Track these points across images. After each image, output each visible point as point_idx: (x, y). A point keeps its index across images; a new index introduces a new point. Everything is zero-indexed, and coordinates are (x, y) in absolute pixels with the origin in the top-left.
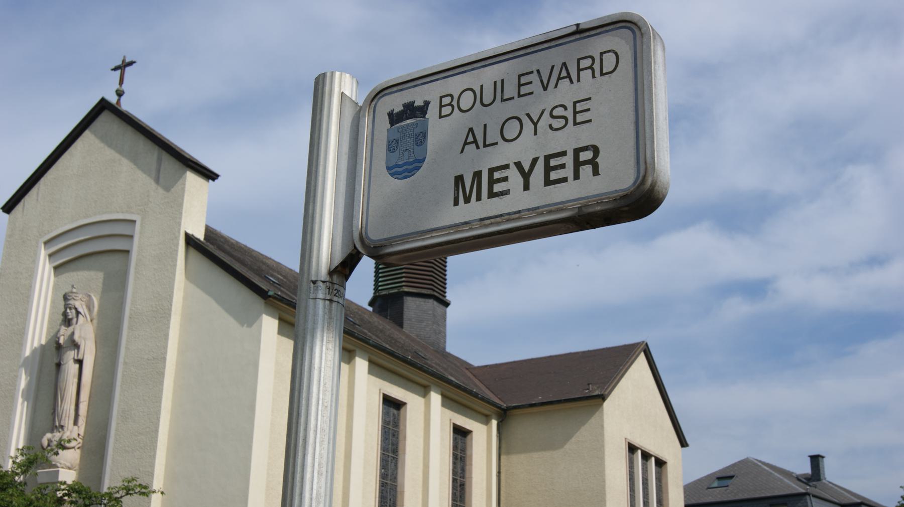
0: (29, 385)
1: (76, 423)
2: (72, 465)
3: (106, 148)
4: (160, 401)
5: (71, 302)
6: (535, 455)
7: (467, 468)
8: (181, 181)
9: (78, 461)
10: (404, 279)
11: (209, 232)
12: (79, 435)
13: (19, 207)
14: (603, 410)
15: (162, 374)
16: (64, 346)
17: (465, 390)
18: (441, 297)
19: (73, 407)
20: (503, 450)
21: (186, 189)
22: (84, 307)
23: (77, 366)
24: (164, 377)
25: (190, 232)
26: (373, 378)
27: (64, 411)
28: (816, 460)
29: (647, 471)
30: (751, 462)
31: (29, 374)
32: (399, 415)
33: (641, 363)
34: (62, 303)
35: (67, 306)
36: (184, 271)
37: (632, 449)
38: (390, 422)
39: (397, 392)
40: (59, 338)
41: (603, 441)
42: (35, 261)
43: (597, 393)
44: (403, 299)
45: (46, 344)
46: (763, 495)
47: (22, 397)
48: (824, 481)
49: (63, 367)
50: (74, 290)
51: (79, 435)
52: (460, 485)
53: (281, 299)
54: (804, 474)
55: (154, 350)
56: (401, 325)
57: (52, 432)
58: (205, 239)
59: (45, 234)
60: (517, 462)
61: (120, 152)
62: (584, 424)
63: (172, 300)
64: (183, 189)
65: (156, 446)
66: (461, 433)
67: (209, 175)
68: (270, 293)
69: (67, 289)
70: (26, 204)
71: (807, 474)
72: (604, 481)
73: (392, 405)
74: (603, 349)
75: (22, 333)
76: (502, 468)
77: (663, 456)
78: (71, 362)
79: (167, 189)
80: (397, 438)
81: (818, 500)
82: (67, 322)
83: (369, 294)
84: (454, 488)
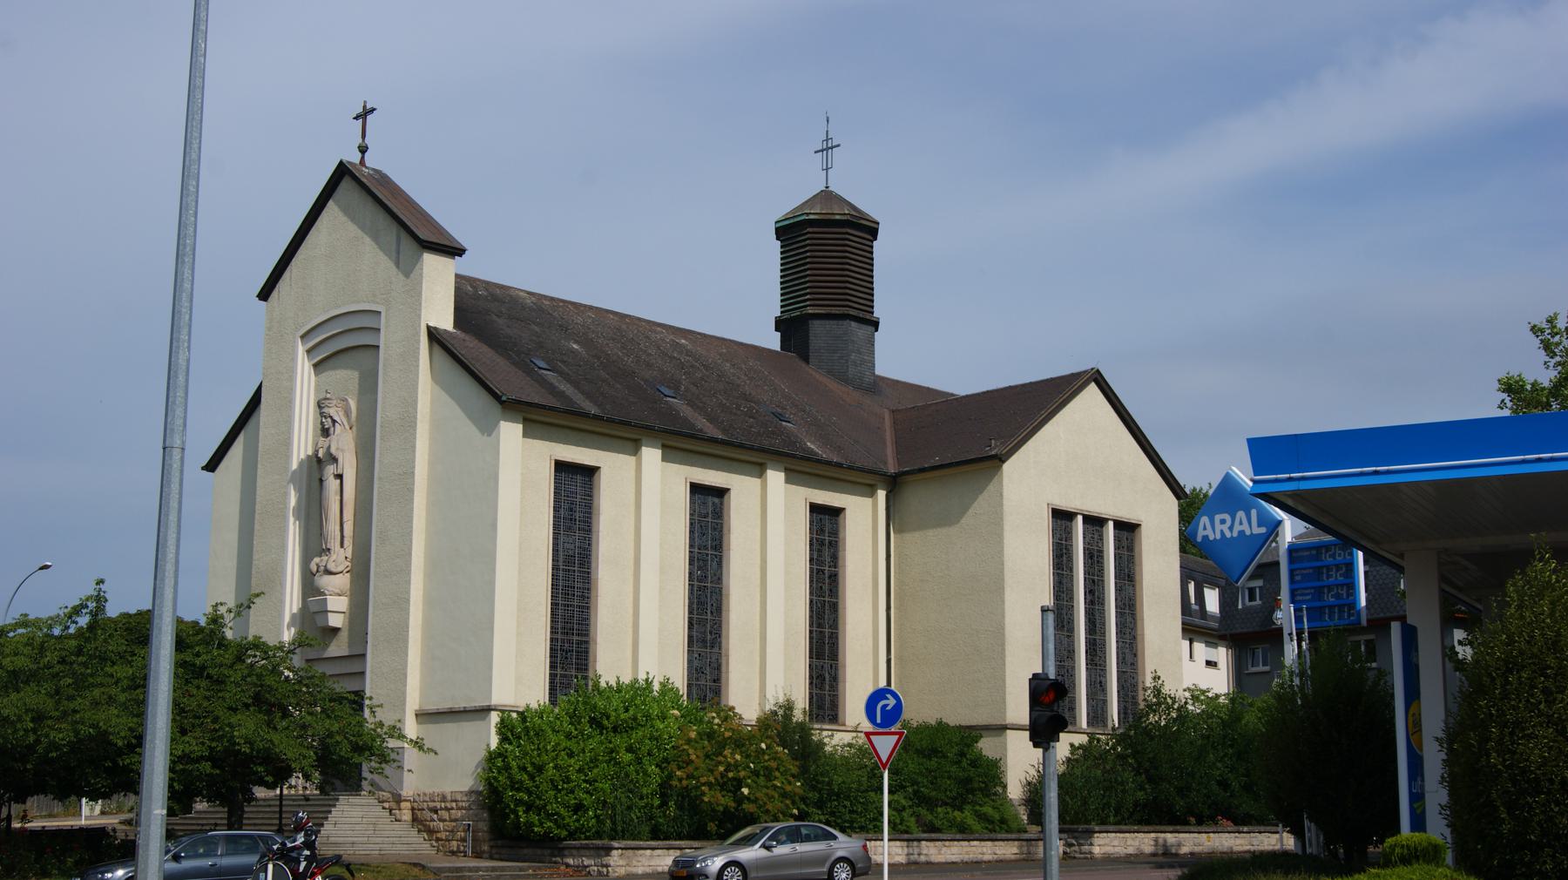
1: (342, 546)
2: (342, 591)
4: (411, 521)
5: (325, 410)
6: (931, 533)
8: (419, 265)
9: (349, 586)
12: (346, 558)
13: (275, 294)
18: (868, 317)
19: (338, 528)
21: (424, 275)
22: (341, 414)
23: (338, 481)
24: (413, 494)
25: (431, 324)
31: (298, 490)
32: (722, 504)
35: (322, 415)
36: (429, 370)
38: (708, 513)
40: (317, 451)
41: (1002, 514)
42: (294, 360)
49: (324, 483)
50: (328, 396)
51: (346, 558)
52: (830, 577)
58: (457, 324)
61: (362, 228)
64: (421, 275)
75: (287, 443)
78: (332, 478)
82: (325, 432)
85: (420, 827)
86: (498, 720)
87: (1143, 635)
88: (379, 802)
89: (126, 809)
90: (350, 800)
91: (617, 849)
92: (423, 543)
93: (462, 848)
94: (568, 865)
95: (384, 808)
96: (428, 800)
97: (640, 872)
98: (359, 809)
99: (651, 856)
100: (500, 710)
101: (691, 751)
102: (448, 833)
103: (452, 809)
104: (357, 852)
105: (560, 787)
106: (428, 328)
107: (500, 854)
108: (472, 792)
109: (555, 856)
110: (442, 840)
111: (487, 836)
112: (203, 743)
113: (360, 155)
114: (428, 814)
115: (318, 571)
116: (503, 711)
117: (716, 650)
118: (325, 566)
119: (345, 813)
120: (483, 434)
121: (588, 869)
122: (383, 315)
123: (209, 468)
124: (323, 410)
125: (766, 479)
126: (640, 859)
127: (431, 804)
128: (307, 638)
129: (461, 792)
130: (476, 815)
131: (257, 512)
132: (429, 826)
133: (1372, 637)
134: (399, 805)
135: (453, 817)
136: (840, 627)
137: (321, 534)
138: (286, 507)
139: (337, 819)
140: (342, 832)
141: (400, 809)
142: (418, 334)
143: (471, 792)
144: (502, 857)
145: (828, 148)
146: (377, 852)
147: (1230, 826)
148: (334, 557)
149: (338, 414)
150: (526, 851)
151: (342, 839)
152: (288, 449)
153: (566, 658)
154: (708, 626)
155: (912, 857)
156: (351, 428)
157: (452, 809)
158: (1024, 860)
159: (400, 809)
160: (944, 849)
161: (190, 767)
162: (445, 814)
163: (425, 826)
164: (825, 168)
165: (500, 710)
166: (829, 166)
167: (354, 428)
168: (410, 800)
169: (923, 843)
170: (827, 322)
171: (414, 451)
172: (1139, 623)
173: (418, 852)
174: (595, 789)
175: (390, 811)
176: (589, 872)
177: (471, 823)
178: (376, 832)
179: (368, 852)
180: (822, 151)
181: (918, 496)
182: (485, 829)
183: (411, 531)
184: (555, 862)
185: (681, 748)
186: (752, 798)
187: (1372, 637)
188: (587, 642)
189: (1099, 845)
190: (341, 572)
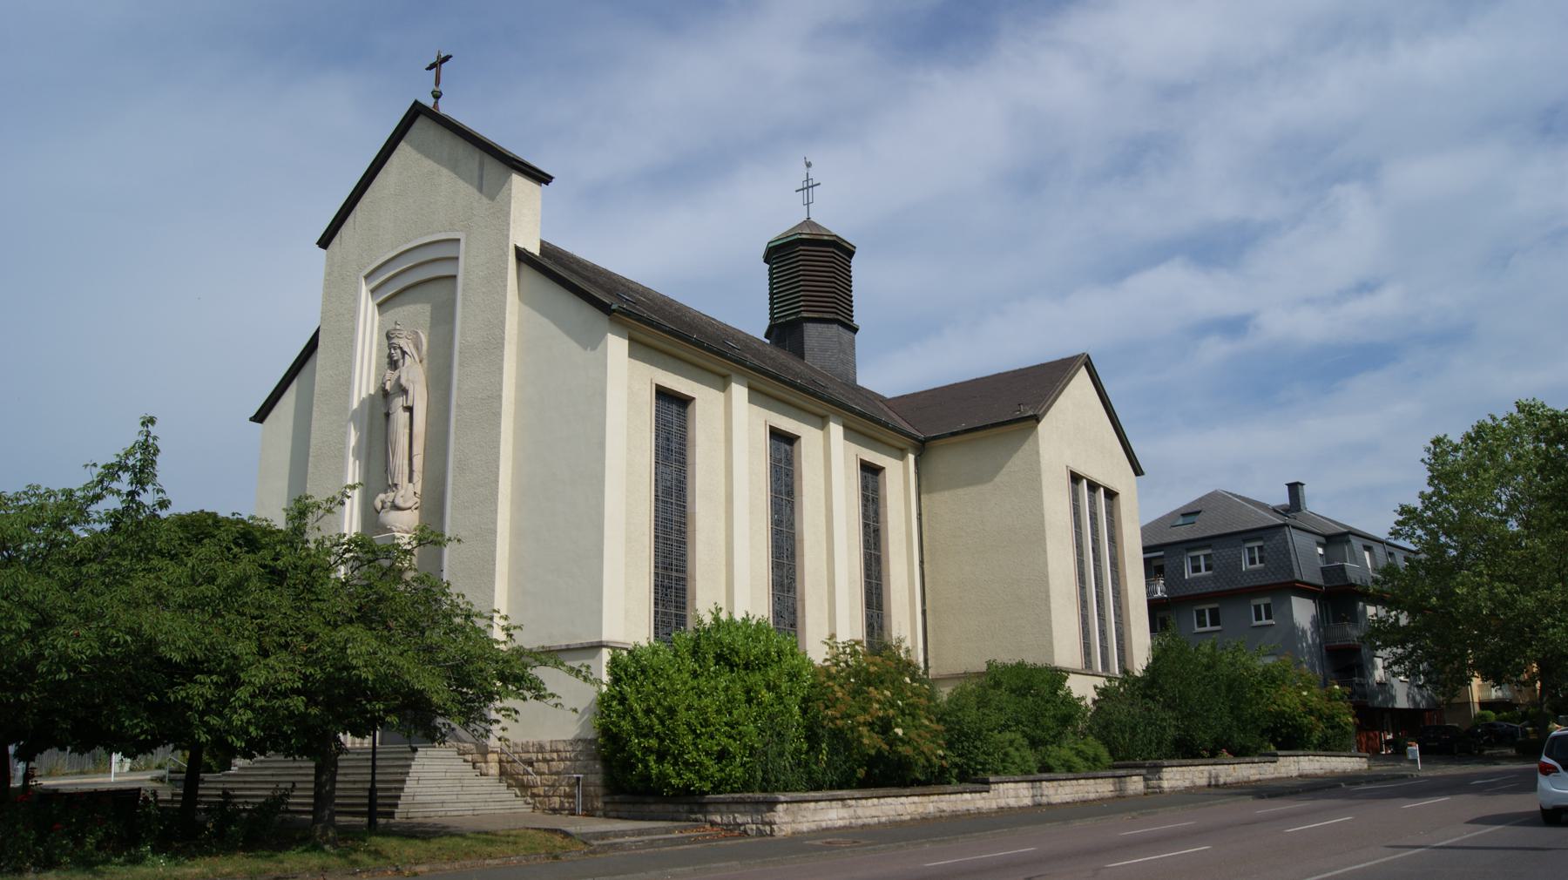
0: (359, 441)
1: (410, 480)
3: (423, 158)
5: (395, 341)
6: (961, 492)
7: (881, 510)
8: (506, 185)
10: (802, 303)
11: (544, 247)
12: (415, 493)
13: (336, 240)
14: (1037, 433)
15: (497, 415)
16: (392, 392)
17: (872, 419)
18: (847, 321)
19: (406, 462)
20: (923, 488)
22: (411, 346)
23: (407, 414)
25: (519, 245)
26: (756, 409)
27: (397, 468)
28: (1294, 488)
29: (1095, 504)
30: (1221, 494)
31: (359, 429)
32: (792, 451)
33: (1081, 382)
34: (385, 342)
35: (391, 346)
37: (1075, 478)
39: (787, 424)
40: (385, 384)
41: (1039, 470)
42: (356, 299)
43: (1030, 413)
44: (803, 327)
45: (375, 393)
46: (1235, 530)
47: (353, 455)
48: (1305, 511)
49: (391, 417)
50: (398, 327)
51: (415, 493)
52: (874, 531)
53: (628, 314)
54: (1282, 506)
55: (488, 388)
56: (802, 357)
57: (386, 492)
59: (365, 267)
60: (943, 502)
61: (439, 161)
62: (1016, 451)
63: (504, 327)
64: (509, 195)
65: (497, 499)
66: (870, 471)
67: (542, 178)
68: (614, 307)
69: (390, 326)
70: (343, 235)
71: (1286, 505)
72: (1043, 516)
73: (782, 440)
74: (1038, 366)
75: (347, 383)
76: (923, 509)
77: (1114, 485)
78: (400, 410)
79: (492, 198)
80: (792, 478)
81: (1299, 532)
82: (393, 365)
83: (765, 322)
84: (866, 534)
85: (510, 781)
86: (609, 658)
87: (1126, 590)
88: (459, 754)
89: (153, 766)
90: (428, 753)
91: (782, 803)
92: (510, 471)
93: (567, 805)
94: (713, 824)
95: (465, 761)
96: (520, 750)
97: (805, 829)
98: (438, 762)
99: (815, 810)
100: (611, 647)
101: (837, 688)
102: (547, 788)
103: (553, 760)
104: (449, 814)
105: (698, 732)
106: (517, 249)
107: (617, 811)
108: (579, 740)
109: (695, 813)
110: (539, 796)
111: (600, 791)
112: (292, 669)
113: (433, 100)
114: (520, 767)
115: (383, 508)
116: (614, 648)
117: (791, 594)
118: (393, 502)
119: (425, 767)
120: (586, 349)
121: (742, 828)
122: (462, 241)
123: (258, 419)
124: (393, 341)
125: (829, 433)
126: (805, 813)
127: (525, 756)
128: (432, 532)
129: (564, 741)
130: (586, 767)
131: (311, 454)
132: (523, 780)
133: (1215, 606)
134: (486, 758)
135: (554, 770)
136: (884, 579)
137: (387, 469)
138: (344, 443)
139: (419, 775)
140: (429, 789)
141: (486, 762)
142: (506, 254)
143: (576, 741)
144: (620, 814)
145: (808, 186)
146: (470, 813)
147: (1230, 758)
148: (402, 492)
149: (409, 347)
150: (653, 807)
151: (429, 798)
152: (348, 389)
153: (666, 595)
154: (785, 570)
155: (1036, 798)
156: (421, 362)
157: (553, 760)
158: (1118, 797)
159: (486, 762)
160: (1060, 789)
161: (277, 703)
162: (544, 767)
163: (516, 780)
164: (806, 202)
165: (611, 647)
166: (810, 201)
167: (425, 362)
168: (497, 752)
169: (1044, 783)
170: (819, 325)
171: (501, 374)
172: (1121, 579)
173: (513, 811)
174: (740, 733)
175: (474, 764)
176: (745, 831)
177: (581, 776)
178: (464, 788)
179: (461, 813)
180: (803, 189)
181: (946, 460)
182: (598, 782)
183: (498, 458)
184: (696, 820)
185: (825, 685)
186: (906, 739)
187: (1215, 606)
188: (684, 579)
189: (1167, 780)
190: (410, 508)
